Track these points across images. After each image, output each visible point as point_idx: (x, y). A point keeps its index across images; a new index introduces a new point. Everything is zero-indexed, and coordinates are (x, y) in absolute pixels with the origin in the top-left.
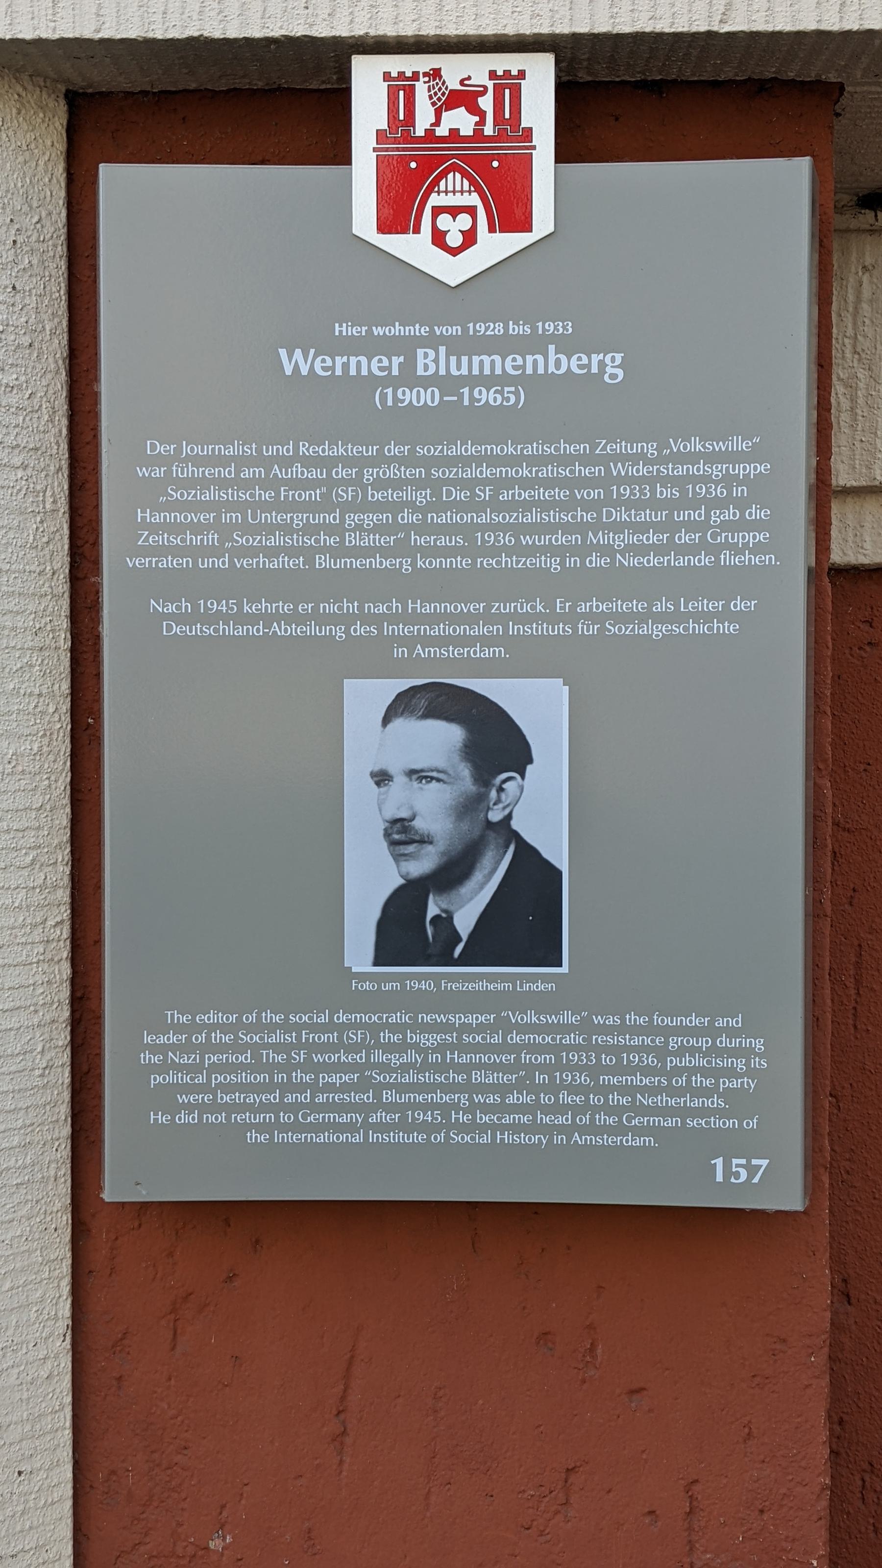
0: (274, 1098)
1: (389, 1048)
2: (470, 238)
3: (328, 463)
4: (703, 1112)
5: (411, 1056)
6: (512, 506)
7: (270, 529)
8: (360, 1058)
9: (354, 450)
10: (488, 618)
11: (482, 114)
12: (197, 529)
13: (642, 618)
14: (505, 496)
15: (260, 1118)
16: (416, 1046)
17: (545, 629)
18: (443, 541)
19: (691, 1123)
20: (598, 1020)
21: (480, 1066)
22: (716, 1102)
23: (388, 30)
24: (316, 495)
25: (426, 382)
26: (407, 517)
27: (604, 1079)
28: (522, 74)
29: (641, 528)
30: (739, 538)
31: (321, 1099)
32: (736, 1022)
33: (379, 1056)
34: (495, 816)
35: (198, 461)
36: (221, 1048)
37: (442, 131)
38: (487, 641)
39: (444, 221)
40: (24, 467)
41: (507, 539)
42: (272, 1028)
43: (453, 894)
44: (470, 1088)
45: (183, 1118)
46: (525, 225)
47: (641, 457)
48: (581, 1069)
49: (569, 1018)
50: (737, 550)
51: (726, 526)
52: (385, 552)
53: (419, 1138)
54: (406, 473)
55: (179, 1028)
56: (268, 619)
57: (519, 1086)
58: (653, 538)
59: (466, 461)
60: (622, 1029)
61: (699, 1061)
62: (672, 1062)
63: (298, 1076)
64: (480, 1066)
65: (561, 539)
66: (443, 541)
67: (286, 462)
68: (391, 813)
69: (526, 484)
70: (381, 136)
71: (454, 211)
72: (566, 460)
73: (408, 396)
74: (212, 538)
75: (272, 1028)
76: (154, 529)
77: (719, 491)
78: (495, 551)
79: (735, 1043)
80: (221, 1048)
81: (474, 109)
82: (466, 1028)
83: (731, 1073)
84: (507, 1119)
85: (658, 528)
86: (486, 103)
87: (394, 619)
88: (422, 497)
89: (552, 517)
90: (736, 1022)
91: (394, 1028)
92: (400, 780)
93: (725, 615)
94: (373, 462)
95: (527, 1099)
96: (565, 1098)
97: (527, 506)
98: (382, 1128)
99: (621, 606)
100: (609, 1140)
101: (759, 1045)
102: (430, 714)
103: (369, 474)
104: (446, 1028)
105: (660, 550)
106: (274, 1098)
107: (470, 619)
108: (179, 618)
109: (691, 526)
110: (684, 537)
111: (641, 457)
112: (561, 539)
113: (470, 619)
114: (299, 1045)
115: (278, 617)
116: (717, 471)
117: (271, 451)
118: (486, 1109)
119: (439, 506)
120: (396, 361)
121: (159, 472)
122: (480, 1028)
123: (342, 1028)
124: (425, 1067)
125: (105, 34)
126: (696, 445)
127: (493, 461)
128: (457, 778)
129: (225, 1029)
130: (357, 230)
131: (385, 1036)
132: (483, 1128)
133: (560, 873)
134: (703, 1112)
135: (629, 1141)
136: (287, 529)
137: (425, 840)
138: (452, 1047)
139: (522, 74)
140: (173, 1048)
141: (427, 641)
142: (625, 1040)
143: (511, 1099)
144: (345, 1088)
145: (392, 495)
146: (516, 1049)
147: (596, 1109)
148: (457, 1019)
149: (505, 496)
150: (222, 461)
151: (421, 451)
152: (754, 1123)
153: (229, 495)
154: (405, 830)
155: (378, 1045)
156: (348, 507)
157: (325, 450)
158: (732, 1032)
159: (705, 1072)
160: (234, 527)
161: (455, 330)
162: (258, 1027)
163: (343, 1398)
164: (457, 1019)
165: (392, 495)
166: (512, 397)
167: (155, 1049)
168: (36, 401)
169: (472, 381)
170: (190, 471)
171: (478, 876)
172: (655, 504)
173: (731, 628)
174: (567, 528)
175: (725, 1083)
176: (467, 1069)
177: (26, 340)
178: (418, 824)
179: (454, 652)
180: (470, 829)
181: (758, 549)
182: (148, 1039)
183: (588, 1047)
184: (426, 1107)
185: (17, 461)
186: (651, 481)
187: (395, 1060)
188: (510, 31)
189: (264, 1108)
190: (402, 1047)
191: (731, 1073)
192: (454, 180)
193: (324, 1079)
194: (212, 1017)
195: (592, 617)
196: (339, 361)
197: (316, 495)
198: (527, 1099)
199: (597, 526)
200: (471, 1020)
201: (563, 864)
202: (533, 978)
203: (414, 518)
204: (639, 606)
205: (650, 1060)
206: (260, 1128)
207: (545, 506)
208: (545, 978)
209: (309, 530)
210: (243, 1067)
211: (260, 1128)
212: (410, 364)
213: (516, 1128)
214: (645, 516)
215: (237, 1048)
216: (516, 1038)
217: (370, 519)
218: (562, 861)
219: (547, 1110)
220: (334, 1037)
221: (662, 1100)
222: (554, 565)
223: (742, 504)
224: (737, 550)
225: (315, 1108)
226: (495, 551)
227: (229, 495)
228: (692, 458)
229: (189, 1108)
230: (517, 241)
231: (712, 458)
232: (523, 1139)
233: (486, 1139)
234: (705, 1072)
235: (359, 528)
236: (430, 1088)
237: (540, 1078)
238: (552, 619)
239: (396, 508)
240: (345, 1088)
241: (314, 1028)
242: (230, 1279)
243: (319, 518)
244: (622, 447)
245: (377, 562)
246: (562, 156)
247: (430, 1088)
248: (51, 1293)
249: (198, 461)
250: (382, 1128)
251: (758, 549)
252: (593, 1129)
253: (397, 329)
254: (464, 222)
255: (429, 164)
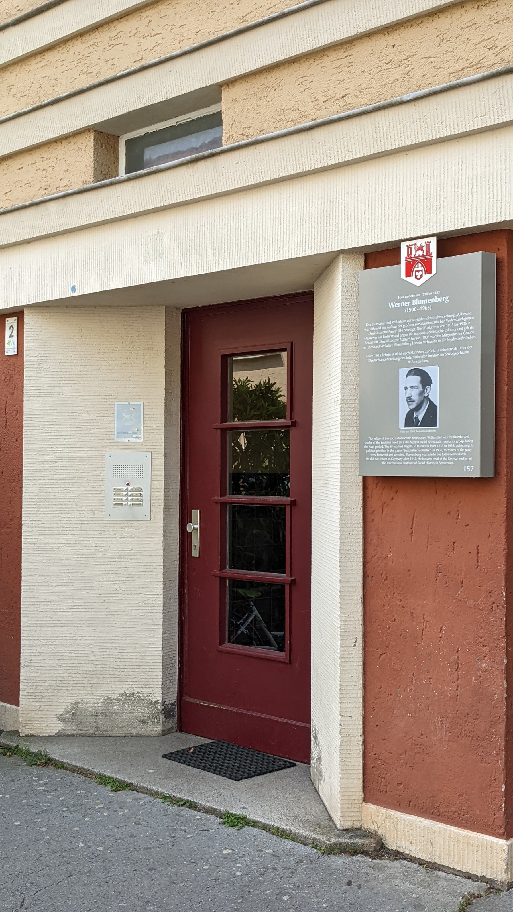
0: (387, 455)
1: (407, 445)
2: (421, 276)
3: (397, 324)
4: (462, 457)
5: (411, 446)
6: (429, 330)
7: (387, 339)
8: (402, 447)
9: (401, 321)
10: (425, 354)
11: (423, 251)
12: (374, 340)
13: (452, 352)
14: (428, 328)
15: (385, 459)
16: (412, 444)
17: (435, 355)
18: (417, 339)
19: (460, 459)
20: (444, 438)
21: (423, 448)
22: (465, 454)
23: (405, 237)
24: (395, 331)
25: (414, 306)
26: (411, 334)
27: (445, 450)
28: (430, 242)
29: (451, 333)
30: (469, 333)
31: (395, 455)
32: (468, 437)
33: (405, 446)
34: (426, 395)
35: (375, 327)
36: (378, 445)
37: (417, 255)
38: (425, 359)
39: (417, 273)
40: (353, 331)
41: (428, 337)
42: (387, 441)
43: (418, 412)
44: (421, 453)
45: (372, 459)
46: (431, 272)
47: (452, 318)
48: (440, 448)
49: (438, 437)
50: (469, 336)
51: (467, 331)
52: (407, 342)
53: (412, 463)
54: (410, 325)
55: (371, 441)
56: (386, 357)
57: (430, 452)
58: (454, 334)
59: (421, 322)
60: (448, 439)
61: (461, 446)
62: (457, 446)
63: (391, 451)
64: (423, 448)
65: (438, 336)
66: (417, 339)
67: (390, 325)
68: (407, 396)
69: (431, 325)
70: (406, 258)
71: (418, 271)
72: (438, 320)
73: (411, 310)
74: (377, 342)
75: (387, 441)
76: (367, 341)
77: (465, 324)
78: (426, 340)
79: (468, 441)
80: (378, 445)
81: (423, 250)
82: (420, 440)
83: (467, 448)
84: (428, 459)
85: (455, 332)
86: (424, 249)
87: (408, 355)
88: (413, 330)
89: (436, 332)
90: (468, 437)
91: (408, 440)
92: (409, 389)
93: (466, 350)
94: (405, 324)
95: (431, 455)
96: (438, 454)
97: (432, 330)
98: (406, 461)
99: (448, 349)
100: (445, 463)
101: (472, 441)
102: (414, 375)
103: (404, 326)
104: (417, 440)
105: (455, 337)
106: (387, 455)
107: (421, 354)
108: (371, 358)
109: (460, 331)
110: (459, 334)
111: (452, 318)
112: (438, 336)
113: (421, 354)
114: (391, 444)
115: (388, 357)
116: (465, 319)
117: (387, 323)
118: (424, 457)
119: (416, 332)
120: (409, 302)
121: (368, 330)
122: (423, 440)
123: (399, 440)
124: (413, 448)
125: (360, 245)
126: (461, 314)
127: (426, 321)
128: (419, 388)
129: (379, 441)
130: (402, 277)
131: (407, 442)
132: (423, 461)
133: (437, 407)
134: (462, 457)
135: (449, 463)
136: (390, 339)
137: (413, 401)
138: (418, 444)
139: (430, 242)
140: (370, 445)
141: (414, 359)
142: (448, 442)
143: (429, 455)
144: (399, 453)
145: (408, 330)
146: (429, 444)
147: (443, 457)
148: (419, 438)
149: (428, 328)
150: (379, 326)
151: (413, 320)
152: (471, 459)
153: (380, 333)
154: (410, 399)
155: (405, 444)
156: (400, 333)
157: (396, 322)
158: (467, 439)
159: (463, 448)
160: (381, 339)
161: (419, 295)
162: (384, 441)
163: (412, 525)
164: (419, 438)
165: (408, 330)
166: (429, 308)
167: (367, 445)
168: (356, 317)
169: (422, 305)
170: (373, 329)
171: (423, 408)
172: (454, 327)
173: (468, 352)
174: (439, 334)
175: (466, 450)
176: (420, 449)
177: (354, 305)
178: (412, 398)
179: (419, 361)
180: (421, 398)
181: (472, 335)
182: (365, 443)
183: (442, 443)
184: (413, 457)
185: (351, 329)
186: (453, 322)
187: (408, 447)
188: (426, 234)
189: (385, 457)
190: (409, 445)
191: (467, 448)
192: (419, 265)
193: (396, 451)
194: (376, 439)
195: (443, 352)
196: (399, 304)
197: (395, 331)
198: (431, 455)
199: (444, 333)
200: (421, 438)
201: (438, 405)
202: (432, 429)
203: (412, 334)
204: (451, 349)
205: (453, 446)
206: (385, 461)
207: (435, 329)
208: (435, 429)
209: (394, 338)
210: (382, 449)
211: (385, 461)
212: (411, 303)
213: (429, 461)
214: (452, 330)
215: (381, 445)
216: (429, 442)
217: (404, 335)
218: (437, 404)
219: (435, 457)
220: (397, 442)
221: (455, 454)
222: (436, 341)
223: (469, 326)
224: (469, 336)
225: (394, 457)
226: (426, 340)
227: (380, 333)
228: (461, 317)
229: (372, 457)
230: (430, 276)
231: (464, 317)
232: (430, 463)
233: (424, 463)
234: (463, 448)
235: (402, 337)
236: (414, 453)
237: (434, 450)
238: (436, 353)
239: (408, 332)
240: (399, 453)
241: (394, 441)
242: (393, 499)
243: (395, 336)
244: (448, 316)
245: (406, 344)
246: (438, 257)
247: (414, 453)
248: (357, 499)
249: (375, 327)
250: (406, 461)
251: (472, 335)
252: (443, 461)
253: (409, 296)
254: (420, 273)
255: (414, 262)
